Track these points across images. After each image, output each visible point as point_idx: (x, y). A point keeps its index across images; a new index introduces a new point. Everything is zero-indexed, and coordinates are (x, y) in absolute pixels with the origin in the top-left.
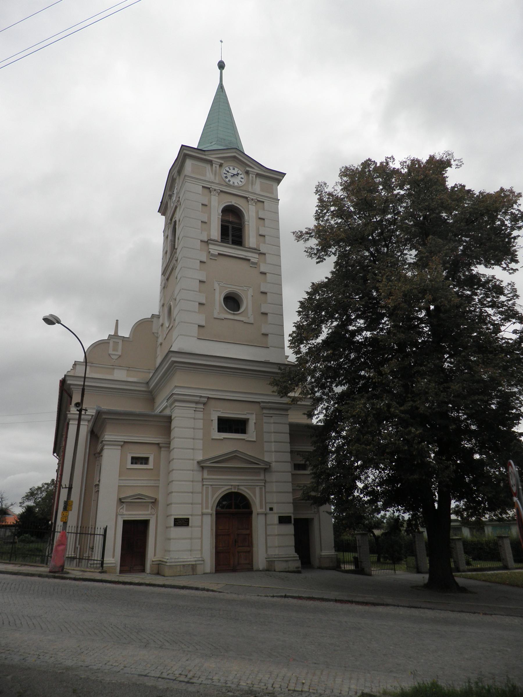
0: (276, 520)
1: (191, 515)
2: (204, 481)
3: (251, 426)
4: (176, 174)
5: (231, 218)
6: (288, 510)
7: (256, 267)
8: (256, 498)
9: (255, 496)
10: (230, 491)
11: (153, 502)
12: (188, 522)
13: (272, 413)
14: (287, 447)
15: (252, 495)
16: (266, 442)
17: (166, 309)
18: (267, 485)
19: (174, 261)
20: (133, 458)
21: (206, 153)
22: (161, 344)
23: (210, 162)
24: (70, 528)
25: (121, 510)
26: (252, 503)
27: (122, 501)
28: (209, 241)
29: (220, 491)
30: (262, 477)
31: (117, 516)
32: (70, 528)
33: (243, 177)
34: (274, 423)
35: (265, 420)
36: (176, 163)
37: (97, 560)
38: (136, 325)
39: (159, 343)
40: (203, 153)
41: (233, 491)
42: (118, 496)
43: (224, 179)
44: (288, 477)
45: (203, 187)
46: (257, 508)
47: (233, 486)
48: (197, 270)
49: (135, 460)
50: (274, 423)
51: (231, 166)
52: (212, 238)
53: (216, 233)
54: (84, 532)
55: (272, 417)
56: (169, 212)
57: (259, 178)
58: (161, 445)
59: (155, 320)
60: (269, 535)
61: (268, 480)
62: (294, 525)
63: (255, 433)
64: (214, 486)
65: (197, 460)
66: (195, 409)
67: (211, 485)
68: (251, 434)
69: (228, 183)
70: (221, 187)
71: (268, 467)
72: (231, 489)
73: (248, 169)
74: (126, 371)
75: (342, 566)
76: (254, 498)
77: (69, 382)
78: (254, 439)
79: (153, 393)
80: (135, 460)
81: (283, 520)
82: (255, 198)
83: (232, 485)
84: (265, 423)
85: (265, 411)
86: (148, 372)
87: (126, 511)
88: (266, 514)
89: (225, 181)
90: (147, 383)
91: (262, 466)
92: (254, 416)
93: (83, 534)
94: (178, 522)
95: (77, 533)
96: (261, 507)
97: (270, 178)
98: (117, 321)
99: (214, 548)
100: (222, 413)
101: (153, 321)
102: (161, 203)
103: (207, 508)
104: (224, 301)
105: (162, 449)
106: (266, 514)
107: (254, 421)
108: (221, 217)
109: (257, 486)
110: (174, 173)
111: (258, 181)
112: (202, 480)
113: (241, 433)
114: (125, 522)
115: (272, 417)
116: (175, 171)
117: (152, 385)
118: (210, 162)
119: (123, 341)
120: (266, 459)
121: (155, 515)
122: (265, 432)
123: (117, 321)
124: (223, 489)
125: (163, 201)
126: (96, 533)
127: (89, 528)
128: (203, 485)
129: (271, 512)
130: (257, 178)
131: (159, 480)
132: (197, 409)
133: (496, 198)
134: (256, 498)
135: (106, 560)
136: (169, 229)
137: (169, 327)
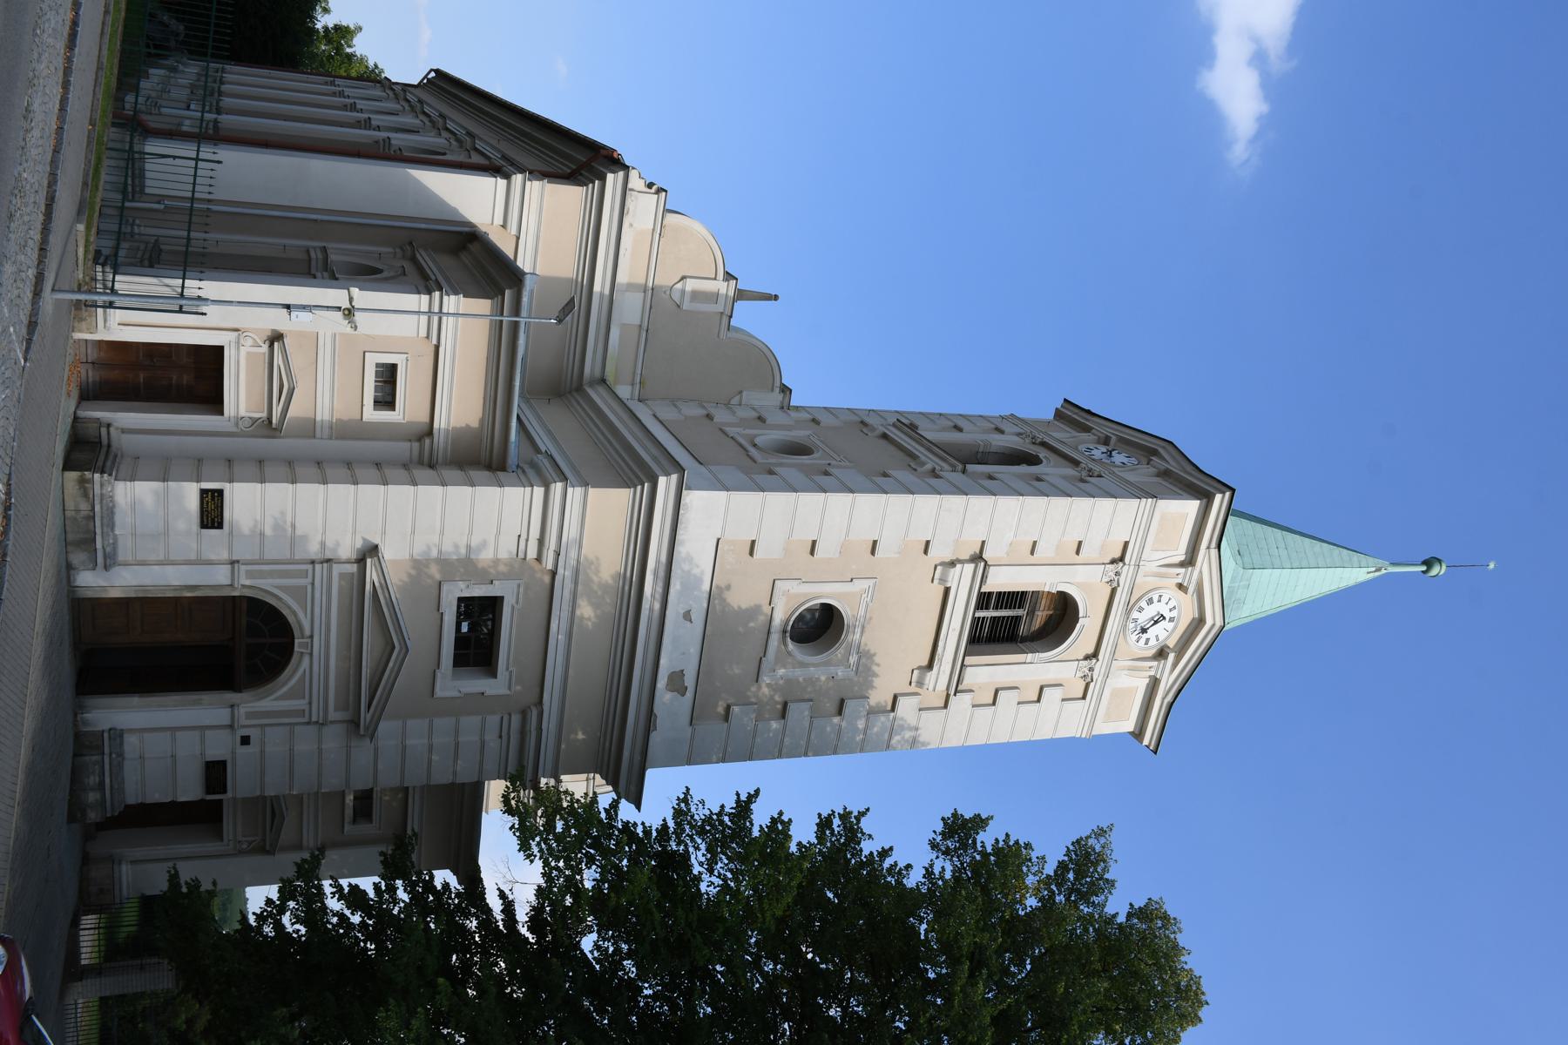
0: (214, 754)
1: (231, 533)
3: (477, 684)
4: (1163, 465)
5: (1041, 616)
6: (241, 784)
7: (910, 684)
8: (275, 699)
10: (296, 633)
11: (270, 422)
12: (213, 527)
14: (415, 779)
15: (285, 689)
17: (800, 435)
18: (312, 729)
19: (931, 462)
20: (392, 368)
21: (1214, 552)
22: (709, 417)
23: (1190, 561)
24: (207, 189)
25: (249, 342)
26: (261, 690)
27: (276, 344)
28: (983, 564)
29: (295, 606)
30: (333, 715)
31: (237, 330)
32: (207, 189)
33: (1150, 644)
34: (483, 743)
35: (493, 720)
36: (1189, 468)
37: (113, 281)
38: (761, 345)
39: (713, 411)
40: (1214, 544)
41: (296, 641)
42: (290, 331)
43: (1146, 598)
44: (332, 782)
45: (1126, 544)
46: (252, 705)
48: (906, 534)
49: (388, 375)
50: (483, 743)
51: (1175, 628)
52: (992, 570)
53: (1000, 581)
54: (191, 180)
55: (501, 737)
56: (1062, 436)
57: (1148, 685)
58: (427, 441)
59: (777, 397)
61: (325, 730)
62: (202, 801)
63: (459, 694)
65: (381, 547)
67: (313, 584)
68: (454, 685)
69: (1136, 607)
70: (1126, 590)
71: (362, 732)
73: (1171, 656)
74: (639, 323)
77: (610, 177)
78: (439, 693)
79: (575, 394)
80: (388, 375)
81: (215, 773)
82: (1121, 584)
83: (311, 637)
84: (484, 722)
85: (516, 720)
86: (634, 379)
87: (248, 353)
88: (231, 727)
89: (1140, 599)
90: (603, 381)
91: (364, 717)
92: (504, 691)
93: (191, 215)
94: (213, 499)
95: (193, 199)
96: (249, 715)
97: (1205, 512)
98: (776, 298)
99: (140, 595)
100: (513, 607)
101: (772, 390)
102: (1088, 412)
103: (250, 575)
104: (823, 604)
105: (416, 445)
106: (231, 727)
107: (489, 692)
108: (1046, 590)
110: (1163, 459)
111: (1142, 684)
112: (328, 561)
113: (455, 655)
114: (218, 351)
115: (501, 737)
116: (1173, 466)
117: (596, 395)
118: (1190, 561)
119: (722, 313)
120: (384, 727)
121: (235, 430)
122: (458, 722)
123: (776, 298)
124: (301, 615)
125: (1095, 419)
126: (190, 194)
127: (206, 232)
128: (313, 562)
129: (238, 740)
130: (1147, 680)
131: (331, 439)
135: (115, 312)
136: (1019, 434)
137: (755, 445)
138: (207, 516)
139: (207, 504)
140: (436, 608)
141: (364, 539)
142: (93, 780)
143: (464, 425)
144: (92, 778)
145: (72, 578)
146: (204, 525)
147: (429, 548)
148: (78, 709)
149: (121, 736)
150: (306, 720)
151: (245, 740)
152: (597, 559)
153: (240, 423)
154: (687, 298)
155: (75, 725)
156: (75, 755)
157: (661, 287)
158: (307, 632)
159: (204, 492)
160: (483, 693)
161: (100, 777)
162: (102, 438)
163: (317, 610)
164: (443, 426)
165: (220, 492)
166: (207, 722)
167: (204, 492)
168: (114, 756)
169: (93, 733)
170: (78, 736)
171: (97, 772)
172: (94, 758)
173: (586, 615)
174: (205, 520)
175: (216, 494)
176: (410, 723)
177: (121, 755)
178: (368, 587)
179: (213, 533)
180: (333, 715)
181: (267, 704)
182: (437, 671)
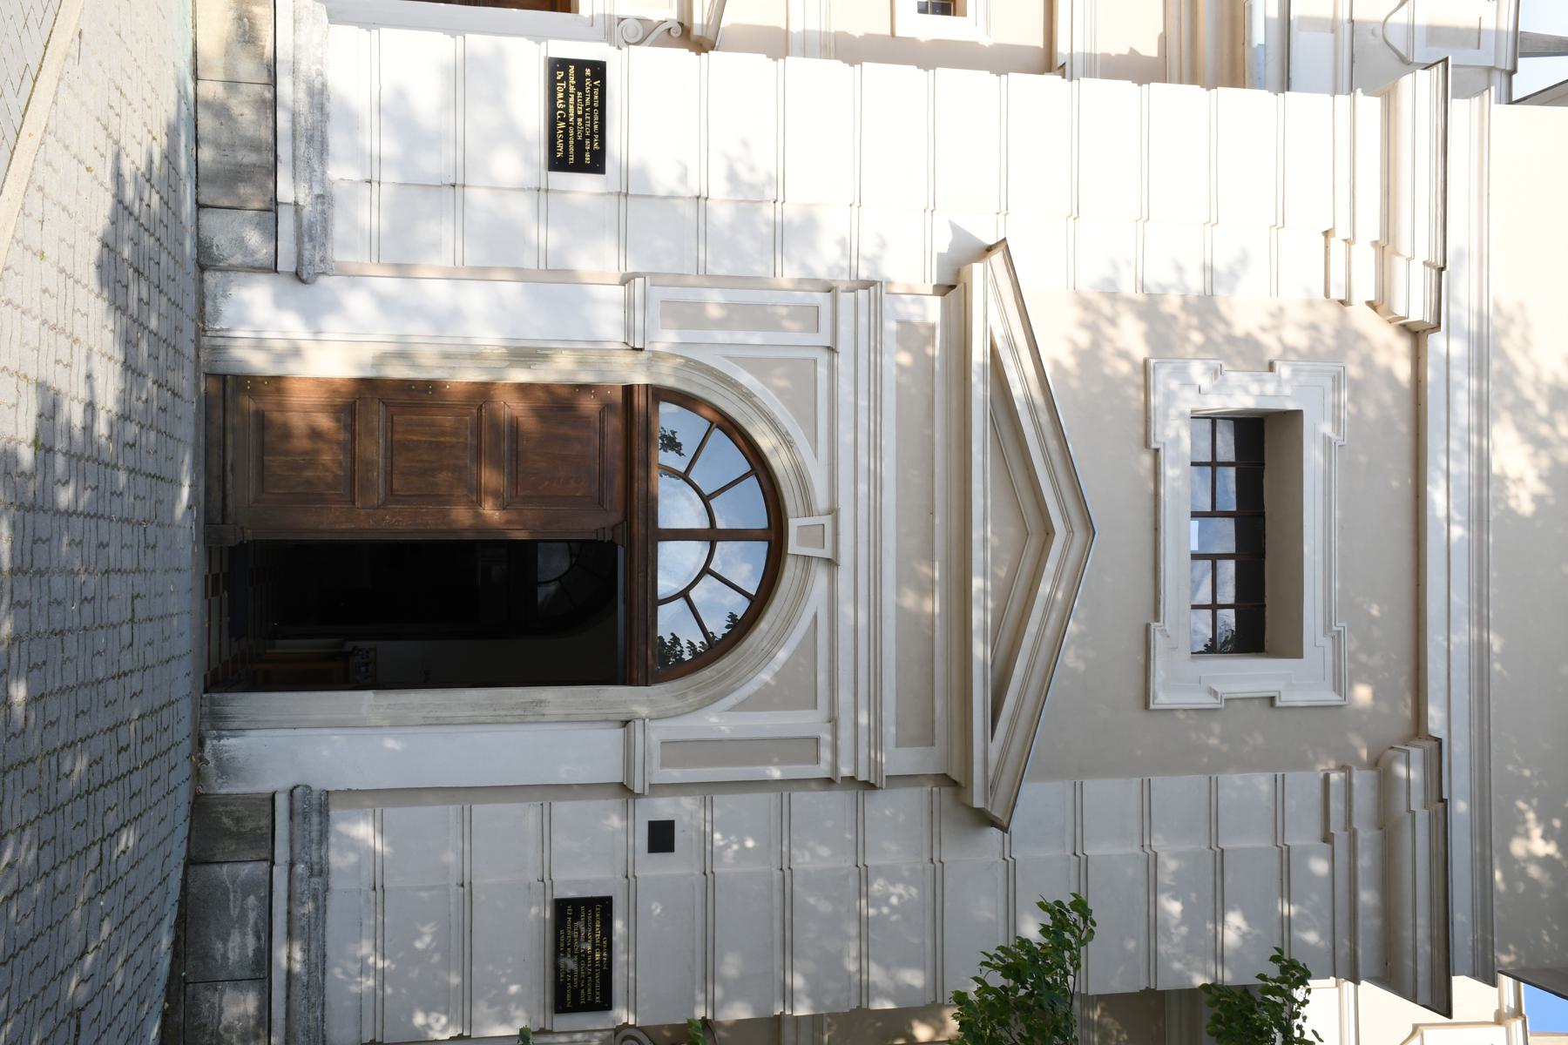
0: (577, 881)
2: (862, 294)
8: (733, 709)
9: (761, 701)
12: (580, 167)
13: (1353, 836)
15: (765, 676)
16: (1146, 790)
18: (839, 799)
41: (791, 522)
47: (826, 520)
60: (467, 821)
63: (1206, 701)
64: (822, 371)
66: (1343, 231)
72: (809, 511)
75: (559, 155)
76: (731, 700)
78: (1162, 698)
85: (1363, 780)
88: (624, 790)
94: (580, 86)
96: (678, 751)
106: (624, 790)
107: (1287, 698)
109: (833, 721)
132: (1337, 245)
133: (241, 961)
134: (733, 709)
138: (566, 131)
139: (566, 98)
140: (1142, 441)
141: (955, 229)
142: (237, 947)
143: (1125, 52)
144: (235, 939)
145: (209, 308)
146: (557, 163)
147: (1071, 341)
148: (210, 723)
149: (324, 811)
150: (823, 770)
151: (661, 837)
152: (1521, 306)
153: (617, 30)
154: (1420, 39)
155: (198, 775)
156: (190, 862)
157: (1364, 23)
158: (821, 500)
159: (557, 67)
160: (1272, 699)
161: (258, 936)
162: (290, 175)
163: (845, 438)
164: (1078, 49)
165: (599, 69)
166: (563, 774)
167: (557, 67)
168: (300, 868)
169: (248, 800)
170: (201, 806)
171: (252, 916)
172: (245, 870)
173: (1512, 472)
174: (560, 146)
175: (588, 72)
176: (1093, 787)
177: (321, 871)
178: (978, 355)
179: (583, 185)
180: (897, 759)
181: (716, 722)
182: (1153, 625)
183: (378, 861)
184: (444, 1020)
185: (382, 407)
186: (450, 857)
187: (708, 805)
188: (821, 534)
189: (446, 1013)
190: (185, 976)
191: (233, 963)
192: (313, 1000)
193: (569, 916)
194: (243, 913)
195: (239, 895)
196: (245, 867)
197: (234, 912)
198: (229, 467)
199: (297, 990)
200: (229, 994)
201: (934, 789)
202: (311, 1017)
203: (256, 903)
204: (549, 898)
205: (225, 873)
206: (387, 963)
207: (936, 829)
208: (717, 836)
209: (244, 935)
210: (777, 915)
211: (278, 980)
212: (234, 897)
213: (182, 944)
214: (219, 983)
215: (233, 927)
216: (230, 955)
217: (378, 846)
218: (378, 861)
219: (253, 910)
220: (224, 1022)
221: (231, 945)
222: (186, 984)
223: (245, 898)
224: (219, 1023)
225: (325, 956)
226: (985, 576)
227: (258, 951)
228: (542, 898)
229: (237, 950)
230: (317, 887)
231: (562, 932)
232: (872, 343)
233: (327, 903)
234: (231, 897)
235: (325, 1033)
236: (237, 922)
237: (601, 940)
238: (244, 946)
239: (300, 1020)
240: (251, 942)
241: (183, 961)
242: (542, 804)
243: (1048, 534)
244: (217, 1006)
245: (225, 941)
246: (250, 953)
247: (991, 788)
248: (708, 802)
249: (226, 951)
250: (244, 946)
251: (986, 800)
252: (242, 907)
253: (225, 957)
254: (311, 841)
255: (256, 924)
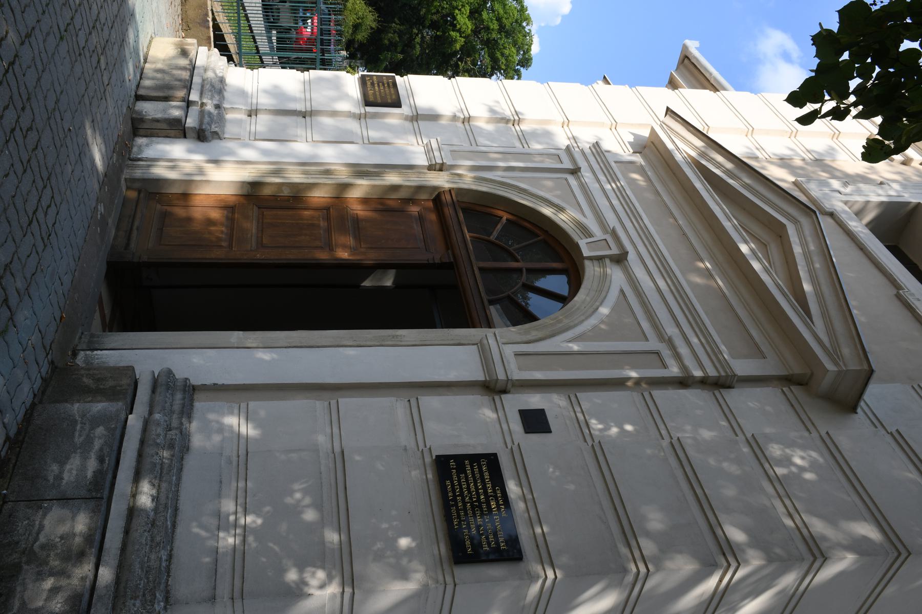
15: (592, 321)
144: (74, 463)
183: (242, 441)
184: (321, 575)
185: (255, 208)
186: (322, 439)
187: (575, 403)
188: (606, 244)
189: (323, 567)
190: (5, 495)
191: (67, 483)
192: (158, 539)
193: (453, 469)
194: (89, 441)
195: (87, 427)
196: (98, 405)
197: (78, 440)
198: (135, 228)
199: (139, 524)
200: (56, 512)
201: (784, 389)
202: (153, 556)
203: (105, 432)
204: (428, 460)
205: (76, 409)
206: (249, 519)
207: (804, 417)
208: (593, 422)
209: (85, 458)
210: (679, 473)
211: (118, 509)
212: (81, 427)
213: (11, 465)
214: (45, 502)
215: (75, 452)
216: (66, 476)
217: (243, 430)
218: (242, 441)
219: (100, 438)
220: (42, 539)
221: (68, 467)
222: (5, 502)
223: (93, 428)
224: (36, 539)
225: (176, 509)
226: (746, 242)
227: (99, 474)
228: (420, 462)
229: (74, 472)
230: (174, 437)
231: (448, 482)
232: (599, 160)
233: (184, 462)
234: (78, 428)
235: (169, 588)
236: (80, 448)
237: (494, 491)
238: (83, 468)
239: (138, 550)
240: (92, 465)
241: (8, 481)
242: (409, 401)
243: (781, 237)
244: (37, 523)
245: (62, 463)
246: (90, 474)
247: (835, 355)
248: (573, 399)
249: (61, 472)
250: (83, 468)
251: (836, 364)
252: (88, 436)
253: (59, 477)
254: (172, 412)
255: (101, 449)
